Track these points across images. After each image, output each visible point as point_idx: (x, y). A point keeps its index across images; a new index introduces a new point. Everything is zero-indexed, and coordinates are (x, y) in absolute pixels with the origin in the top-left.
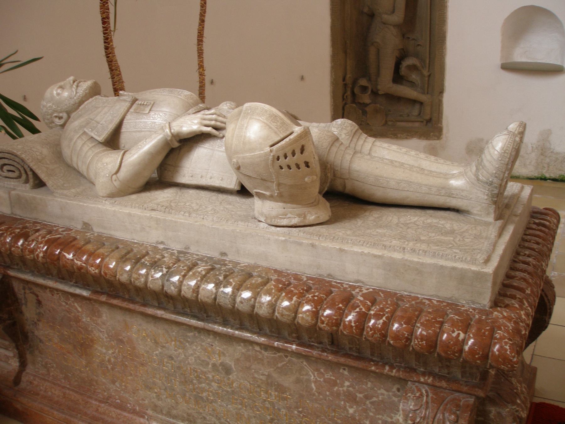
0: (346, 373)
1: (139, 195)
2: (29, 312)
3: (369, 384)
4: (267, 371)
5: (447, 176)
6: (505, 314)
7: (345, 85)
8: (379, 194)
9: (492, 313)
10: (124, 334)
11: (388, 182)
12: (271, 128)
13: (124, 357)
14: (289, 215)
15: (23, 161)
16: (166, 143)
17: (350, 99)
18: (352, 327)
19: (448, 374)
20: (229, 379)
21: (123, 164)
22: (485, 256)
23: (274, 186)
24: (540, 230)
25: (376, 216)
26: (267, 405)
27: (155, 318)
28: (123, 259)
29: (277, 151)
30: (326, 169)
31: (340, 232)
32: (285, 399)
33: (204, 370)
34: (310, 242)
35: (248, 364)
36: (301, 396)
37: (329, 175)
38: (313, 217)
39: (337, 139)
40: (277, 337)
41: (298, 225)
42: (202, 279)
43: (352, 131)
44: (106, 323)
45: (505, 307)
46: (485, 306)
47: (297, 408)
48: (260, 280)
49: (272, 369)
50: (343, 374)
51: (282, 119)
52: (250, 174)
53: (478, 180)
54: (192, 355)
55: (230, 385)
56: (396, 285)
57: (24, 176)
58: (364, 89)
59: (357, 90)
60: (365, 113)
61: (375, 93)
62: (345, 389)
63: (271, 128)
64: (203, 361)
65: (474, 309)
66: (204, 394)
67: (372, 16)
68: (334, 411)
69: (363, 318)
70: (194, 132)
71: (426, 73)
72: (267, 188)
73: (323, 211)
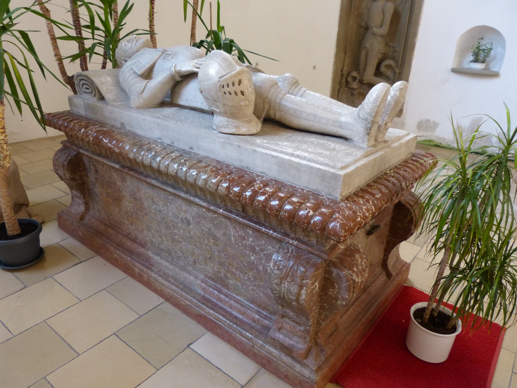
0: (250, 232)
2: (92, 176)
3: (263, 242)
4: (209, 225)
5: (340, 114)
6: (348, 205)
7: (342, 75)
9: (340, 203)
10: (138, 195)
13: (137, 209)
14: (230, 126)
15: (93, 82)
16: (172, 77)
17: (344, 84)
18: (247, 198)
19: (308, 241)
20: (189, 228)
22: (343, 165)
23: (222, 107)
24: (413, 164)
26: (208, 248)
27: (154, 186)
28: (134, 145)
32: (217, 245)
33: (177, 221)
34: (238, 144)
35: (199, 220)
36: (226, 244)
37: (266, 106)
40: (214, 204)
42: (172, 161)
44: (129, 185)
45: (352, 202)
46: (337, 198)
47: (224, 252)
48: (204, 164)
49: (211, 225)
50: (249, 233)
51: (230, 61)
52: (207, 96)
53: (359, 117)
54: (171, 211)
55: (190, 232)
56: (284, 177)
57: (94, 93)
58: (354, 78)
59: (350, 79)
60: (352, 95)
61: (361, 82)
62: (250, 243)
63: (221, 66)
64: (176, 215)
65: (329, 199)
66: (176, 237)
67: (367, 28)
68: (243, 256)
69: (255, 193)
70: (189, 71)
71: (397, 71)
72: (217, 107)
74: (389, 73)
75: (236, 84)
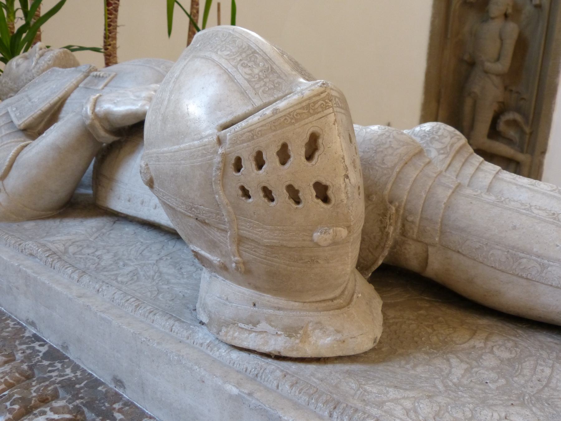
1: (41, 223)
8: (514, 294)
11: (544, 267)
12: (231, 79)
21: (15, 164)
23: (230, 247)
25: (506, 355)
29: (234, 143)
30: (384, 215)
31: (395, 401)
37: (391, 230)
38: (328, 340)
39: (420, 153)
41: (284, 354)
43: (452, 145)
51: (267, 59)
63: (231, 79)
67: (472, 64)
71: (527, 130)
72: (213, 246)
73: (363, 320)
74: (512, 133)
75: (297, 152)
